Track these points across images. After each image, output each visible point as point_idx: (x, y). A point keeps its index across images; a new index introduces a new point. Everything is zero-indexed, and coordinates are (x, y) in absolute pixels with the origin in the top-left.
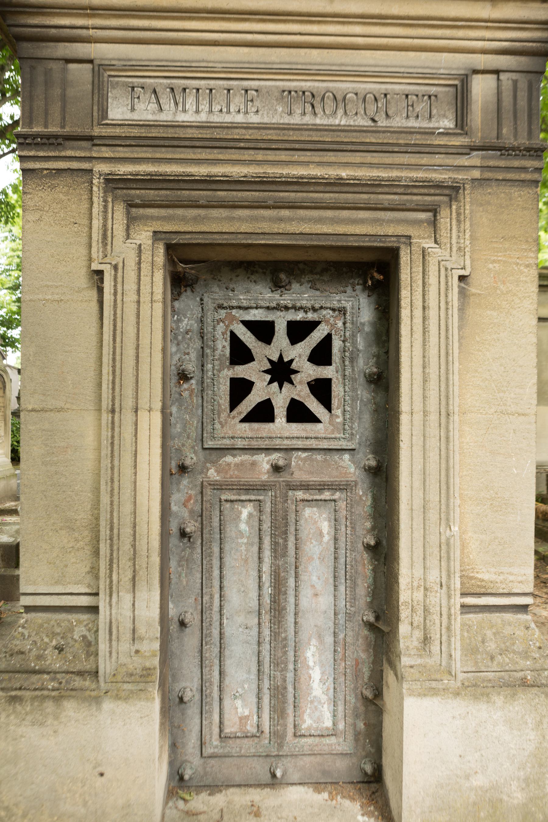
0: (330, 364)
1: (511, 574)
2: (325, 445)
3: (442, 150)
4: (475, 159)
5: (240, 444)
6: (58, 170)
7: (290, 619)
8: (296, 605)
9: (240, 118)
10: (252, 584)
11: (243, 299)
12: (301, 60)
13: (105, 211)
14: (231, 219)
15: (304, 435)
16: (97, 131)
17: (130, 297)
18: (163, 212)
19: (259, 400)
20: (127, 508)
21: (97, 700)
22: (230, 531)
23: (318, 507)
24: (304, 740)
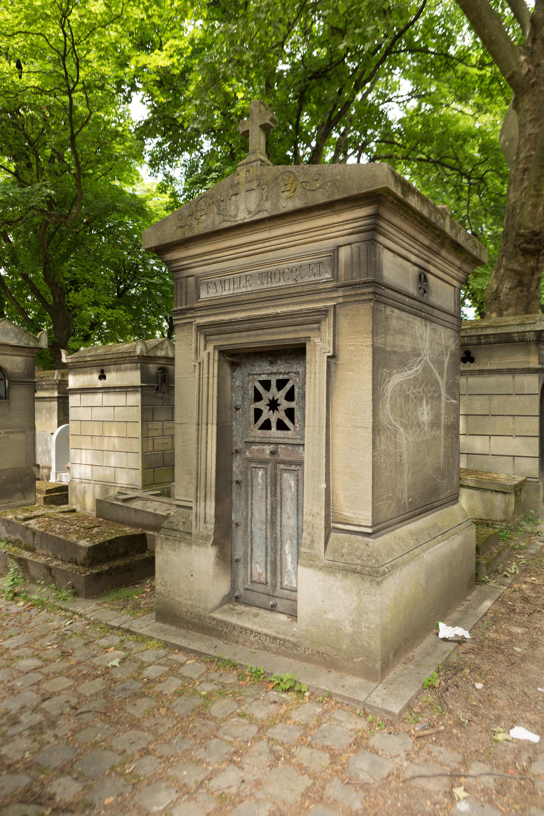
0: (294, 401)
1: (360, 514)
2: (291, 442)
3: (324, 291)
4: (340, 293)
5: (257, 440)
6: (186, 323)
7: (278, 528)
8: (281, 521)
9: (244, 290)
10: (263, 509)
11: (257, 370)
12: (265, 258)
13: (197, 340)
14: (240, 337)
15: (283, 436)
16: (196, 305)
17: (205, 375)
18: (217, 337)
19: (265, 419)
20: (203, 466)
21: (190, 544)
22: (255, 483)
23: (290, 473)
24: (285, 591)
